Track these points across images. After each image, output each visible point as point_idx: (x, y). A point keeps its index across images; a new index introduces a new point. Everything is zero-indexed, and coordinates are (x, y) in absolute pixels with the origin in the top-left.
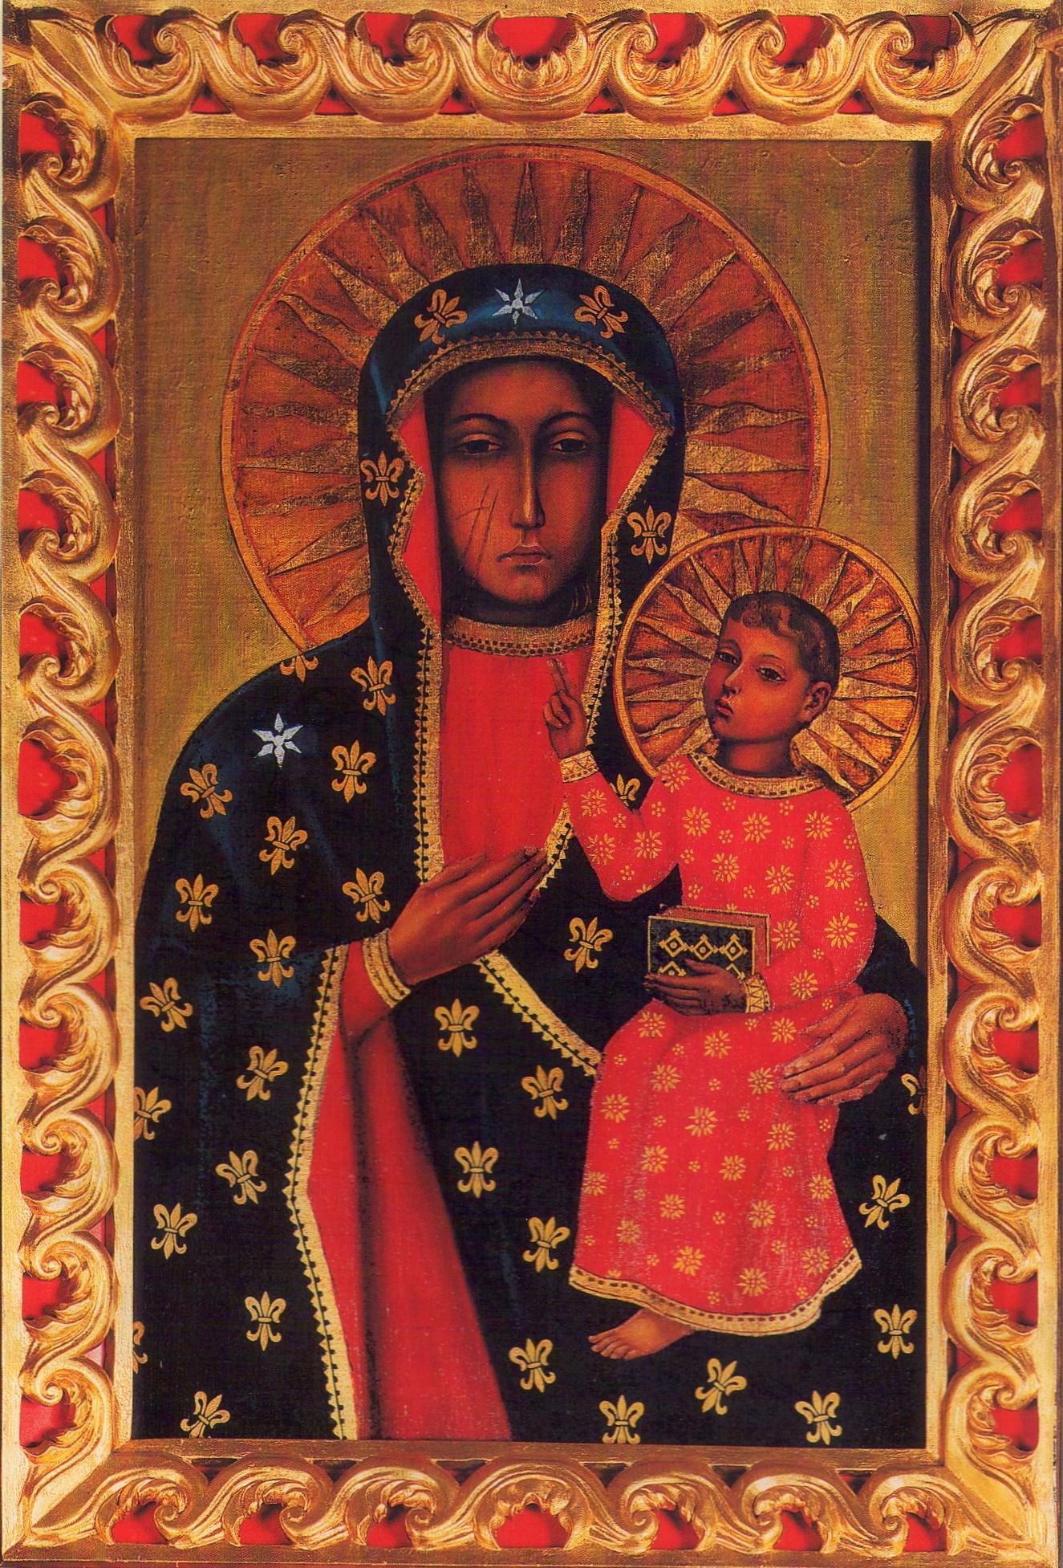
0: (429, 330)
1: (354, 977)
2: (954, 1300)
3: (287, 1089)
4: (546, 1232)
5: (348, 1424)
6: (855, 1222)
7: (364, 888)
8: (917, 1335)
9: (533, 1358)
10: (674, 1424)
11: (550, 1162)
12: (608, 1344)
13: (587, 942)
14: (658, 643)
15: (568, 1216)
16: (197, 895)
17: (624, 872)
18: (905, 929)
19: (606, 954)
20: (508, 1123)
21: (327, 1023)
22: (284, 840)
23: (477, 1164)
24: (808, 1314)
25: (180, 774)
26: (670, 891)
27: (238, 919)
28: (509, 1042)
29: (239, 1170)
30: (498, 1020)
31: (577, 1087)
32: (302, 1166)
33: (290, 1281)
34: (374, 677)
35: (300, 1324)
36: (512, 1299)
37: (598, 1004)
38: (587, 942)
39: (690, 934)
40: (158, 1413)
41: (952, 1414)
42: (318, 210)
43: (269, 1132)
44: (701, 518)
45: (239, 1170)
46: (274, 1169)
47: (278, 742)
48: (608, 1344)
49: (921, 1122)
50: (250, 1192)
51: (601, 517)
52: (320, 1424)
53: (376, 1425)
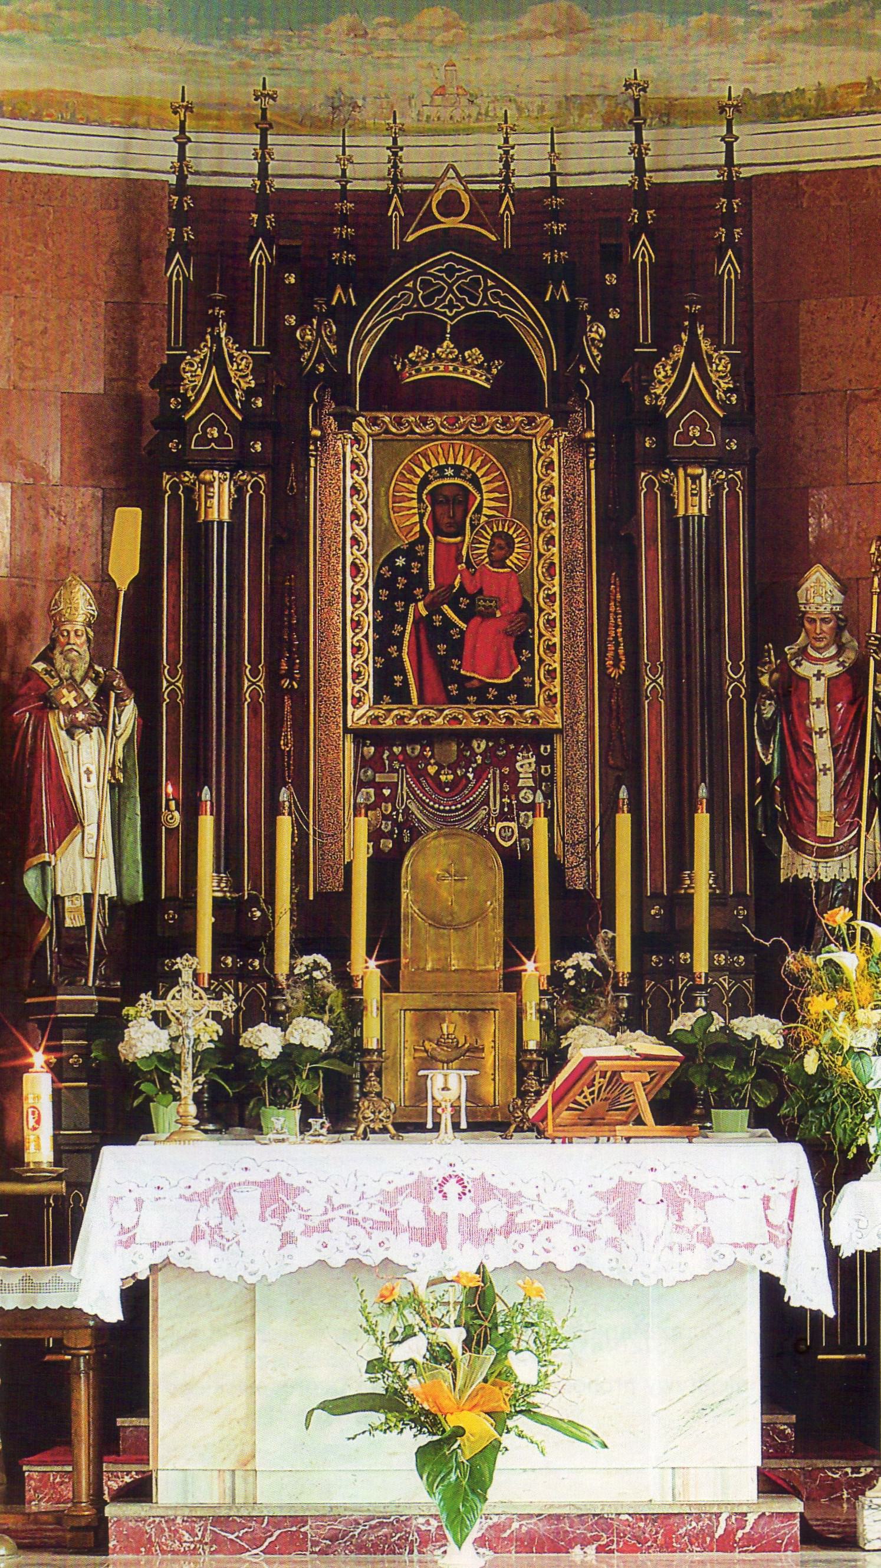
0: (431, 477)
1: (416, 610)
2: (539, 673)
3: (403, 633)
4: (456, 662)
5: (415, 701)
6: (519, 660)
7: (418, 591)
8: (533, 683)
9: (453, 688)
10: (482, 700)
11: (457, 648)
12: (468, 685)
13: (464, 602)
14: (457, 451)
15: (460, 659)
16: (384, 593)
17: (471, 589)
18: (529, 599)
19: (467, 605)
20: (446, 639)
21: (411, 619)
22: (401, 582)
23: (442, 648)
24: (510, 679)
25: (380, 569)
26: (480, 592)
27: (392, 598)
28: (447, 623)
29: (393, 650)
30: (446, 619)
31: (462, 632)
32: (405, 649)
33: (403, 672)
34: (419, 548)
35: (405, 681)
36: (448, 676)
37: (465, 616)
38: (464, 602)
39: (485, 601)
40: (377, 700)
41: (540, 699)
42: (302, 1025)
43: (399, 642)
44: (486, 515)
45: (393, 650)
46: (400, 650)
47: (400, 562)
48: (468, 685)
49: (533, 639)
50: (395, 654)
51: (466, 516)
52: (411, 703)
53: (422, 700)
